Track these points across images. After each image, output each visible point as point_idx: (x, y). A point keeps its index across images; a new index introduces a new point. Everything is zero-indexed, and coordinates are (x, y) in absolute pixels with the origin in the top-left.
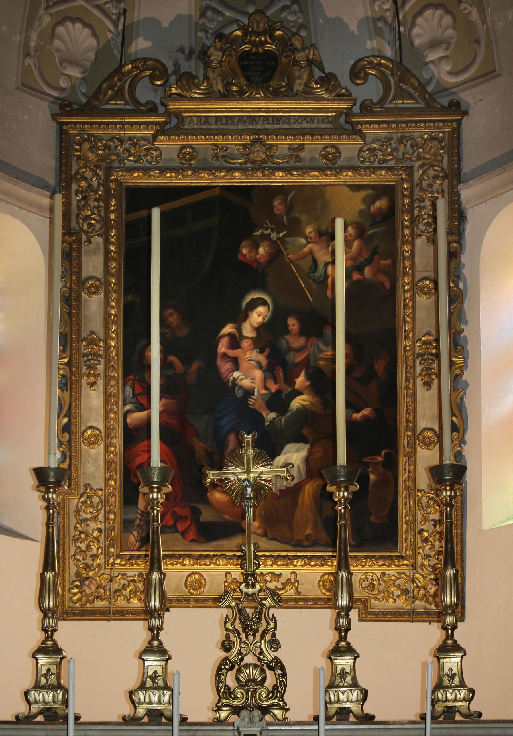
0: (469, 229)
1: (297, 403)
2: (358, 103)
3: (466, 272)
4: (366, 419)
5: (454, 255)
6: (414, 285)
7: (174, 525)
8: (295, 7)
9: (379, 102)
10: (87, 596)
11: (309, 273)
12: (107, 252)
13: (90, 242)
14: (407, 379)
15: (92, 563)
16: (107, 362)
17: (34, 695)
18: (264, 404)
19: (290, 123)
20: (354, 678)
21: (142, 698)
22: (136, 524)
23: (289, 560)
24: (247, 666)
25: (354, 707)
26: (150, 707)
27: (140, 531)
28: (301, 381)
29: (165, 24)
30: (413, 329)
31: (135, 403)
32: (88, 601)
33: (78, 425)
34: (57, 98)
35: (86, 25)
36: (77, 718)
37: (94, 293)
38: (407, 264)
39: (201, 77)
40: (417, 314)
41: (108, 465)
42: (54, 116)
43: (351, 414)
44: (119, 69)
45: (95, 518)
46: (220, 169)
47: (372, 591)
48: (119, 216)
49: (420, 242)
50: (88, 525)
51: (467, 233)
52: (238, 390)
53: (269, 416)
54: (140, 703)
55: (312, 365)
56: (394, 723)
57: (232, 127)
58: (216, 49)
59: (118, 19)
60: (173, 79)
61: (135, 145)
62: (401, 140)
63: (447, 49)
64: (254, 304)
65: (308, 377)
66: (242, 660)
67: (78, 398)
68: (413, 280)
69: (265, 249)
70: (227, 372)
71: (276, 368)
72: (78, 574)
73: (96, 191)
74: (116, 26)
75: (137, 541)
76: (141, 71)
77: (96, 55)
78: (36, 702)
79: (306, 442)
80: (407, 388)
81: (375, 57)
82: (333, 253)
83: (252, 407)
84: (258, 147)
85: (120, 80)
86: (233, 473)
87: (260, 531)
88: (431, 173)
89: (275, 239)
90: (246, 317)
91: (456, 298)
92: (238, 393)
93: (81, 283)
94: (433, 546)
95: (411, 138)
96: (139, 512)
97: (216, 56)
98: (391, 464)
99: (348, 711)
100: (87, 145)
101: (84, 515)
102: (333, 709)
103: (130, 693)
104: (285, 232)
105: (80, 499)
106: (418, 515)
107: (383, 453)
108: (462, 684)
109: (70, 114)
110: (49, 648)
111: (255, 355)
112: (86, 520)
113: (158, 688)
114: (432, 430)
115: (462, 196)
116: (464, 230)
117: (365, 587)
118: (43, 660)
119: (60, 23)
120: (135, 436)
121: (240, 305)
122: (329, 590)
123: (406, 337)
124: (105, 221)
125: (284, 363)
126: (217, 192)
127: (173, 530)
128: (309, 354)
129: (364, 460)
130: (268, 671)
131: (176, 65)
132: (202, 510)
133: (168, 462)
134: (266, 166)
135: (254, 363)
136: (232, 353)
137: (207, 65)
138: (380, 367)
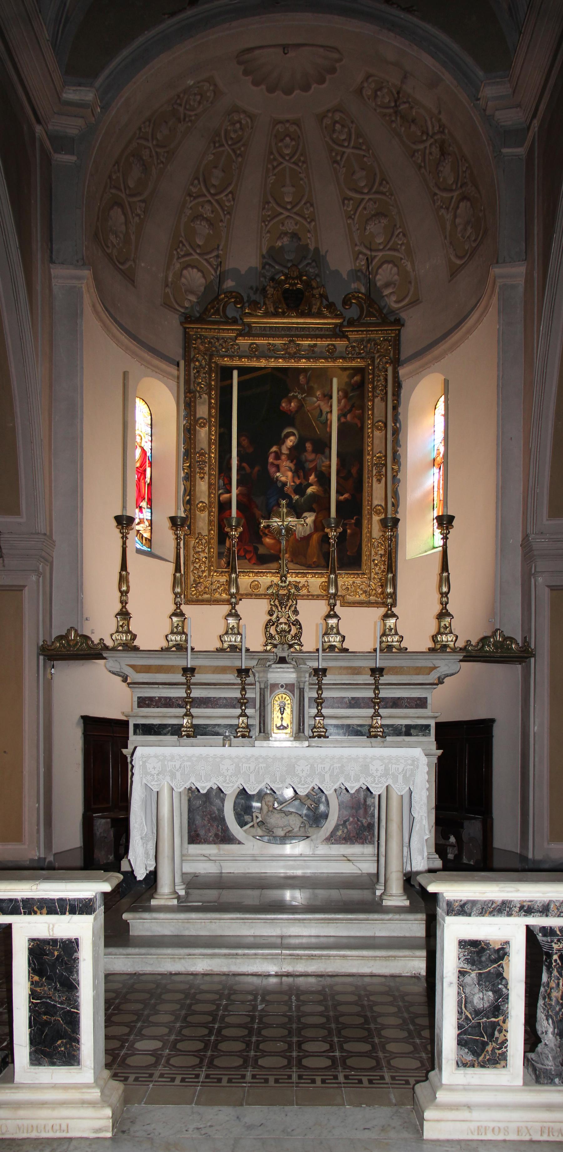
0: (403, 392)
1: (310, 490)
2: (347, 319)
3: (401, 417)
4: (346, 500)
5: (395, 408)
6: (373, 424)
7: (245, 556)
8: (314, 264)
9: (358, 319)
10: (200, 592)
12: (210, 403)
13: (201, 398)
14: (368, 478)
16: (210, 466)
17: (170, 637)
19: (309, 331)
20: (338, 630)
21: (226, 639)
23: (304, 575)
24: (281, 624)
25: (338, 644)
26: (231, 643)
28: (312, 478)
29: (243, 272)
30: (372, 449)
32: (200, 595)
33: (194, 500)
34: (183, 313)
35: (199, 270)
36: (192, 649)
37: (203, 427)
38: (369, 431)
39: (262, 304)
40: (374, 441)
41: (210, 522)
42: (182, 323)
44: (217, 298)
45: (203, 551)
46: (271, 357)
48: (216, 383)
49: (377, 400)
51: (402, 395)
54: (225, 641)
55: (318, 469)
56: (359, 652)
57: (278, 333)
58: (270, 287)
59: (217, 268)
60: (247, 305)
61: (225, 342)
62: (369, 341)
63: (394, 287)
64: (288, 435)
65: (316, 476)
66: (279, 620)
67: (195, 485)
68: (373, 422)
72: (195, 581)
73: (204, 368)
74: (216, 272)
76: (229, 299)
77: (205, 288)
78: (172, 641)
79: (314, 512)
80: (368, 482)
81: (356, 292)
82: (331, 406)
84: (292, 345)
85: (218, 303)
86: (275, 522)
88: (384, 360)
90: (283, 442)
91: (396, 432)
93: (196, 421)
94: (380, 568)
95: (374, 340)
97: (270, 291)
98: (359, 524)
99: (335, 646)
100: (199, 341)
101: (198, 550)
102: (326, 645)
103: (220, 636)
106: (373, 553)
108: (396, 634)
109: (190, 322)
110: (178, 613)
112: (199, 552)
113: (235, 634)
114: (381, 506)
115: (400, 374)
116: (400, 394)
118: (175, 619)
119: (185, 268)
120: (224, 507)
121: (281, 435)
122: (325, 591)
123: (369, 454)
124: (209, 386)
125: (303, 468)
126: (270, 371)
130: (292, 626)
131: (249, 297)
134: (296, 356)
136: (276, 462)
137: (265, 297)
138: (354, 471)
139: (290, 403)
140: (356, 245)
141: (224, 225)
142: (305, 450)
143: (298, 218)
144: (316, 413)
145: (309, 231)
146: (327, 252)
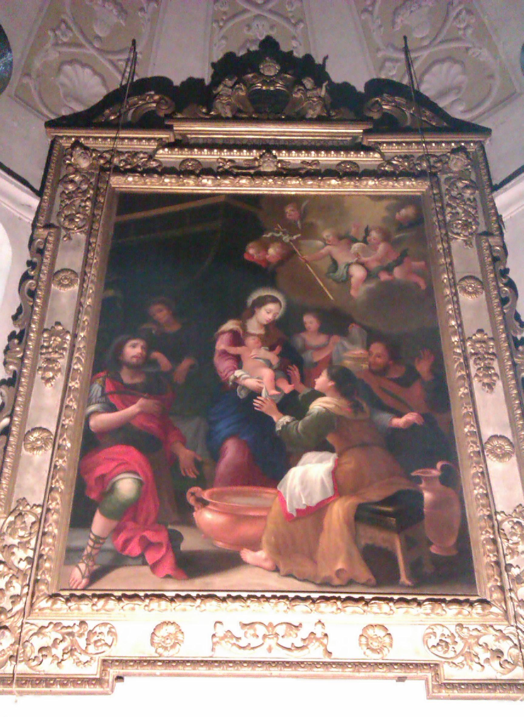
7: (142, 556)
11: (329, 273)
13: (70, 238)
15: (11, 607)
18: (274, 407)
22: (85, 553)
27: (90, 563)
28: (322, 381)
31: (103, 403)
35: (95, 72)
43: (391, 420)
45: (23, 545)
47: (446, 652)
50: (13, 553)
52: (240, 390)
53: (281, 420)
64: (261, 302)
65: (332, 377)
69: (275, 250)
70: (227, 371)
71: (289, 367)
75: (83, 577)
79: (330, 449)
83: (258, 409)
87: (268, 564)
89: (288, 241)
90: (252, 314)
92: (240, 394)
96: (92, 537)
104: (299, 235)
105: (7, 518)
107: (439, 465)
111: (264, 353)
112: (12, 546)
117: (434, 646)
119: (71, 62)
125: (299, 363)
126: (222, 199)
127: (140, 561)
128: (331, 353)
129: (414, 474)
132: (183, 534)
133: (139, 472)
135: (261, 361)
136: (233, 350)
138: (423, 368)
139: (266, 249)
140: (378, 50)
141: (147, 16)
142: (302, 328)
143: (274, 18)
144: (324, 265)
145: (294, 38)
146: (326, 58)
